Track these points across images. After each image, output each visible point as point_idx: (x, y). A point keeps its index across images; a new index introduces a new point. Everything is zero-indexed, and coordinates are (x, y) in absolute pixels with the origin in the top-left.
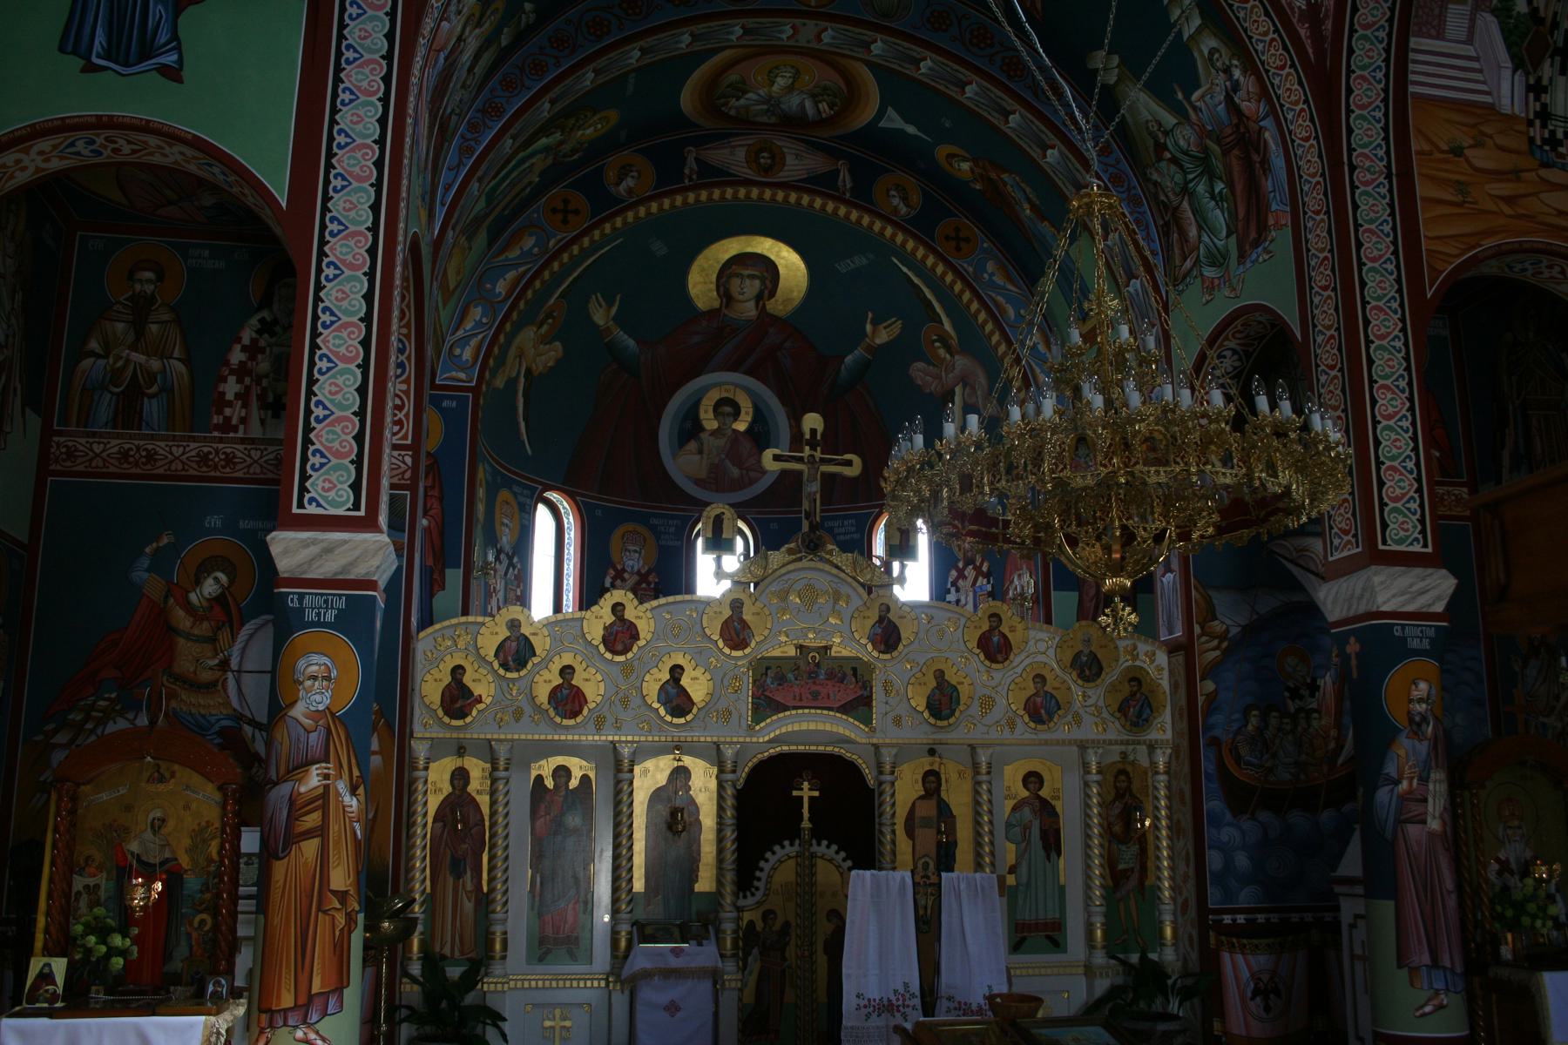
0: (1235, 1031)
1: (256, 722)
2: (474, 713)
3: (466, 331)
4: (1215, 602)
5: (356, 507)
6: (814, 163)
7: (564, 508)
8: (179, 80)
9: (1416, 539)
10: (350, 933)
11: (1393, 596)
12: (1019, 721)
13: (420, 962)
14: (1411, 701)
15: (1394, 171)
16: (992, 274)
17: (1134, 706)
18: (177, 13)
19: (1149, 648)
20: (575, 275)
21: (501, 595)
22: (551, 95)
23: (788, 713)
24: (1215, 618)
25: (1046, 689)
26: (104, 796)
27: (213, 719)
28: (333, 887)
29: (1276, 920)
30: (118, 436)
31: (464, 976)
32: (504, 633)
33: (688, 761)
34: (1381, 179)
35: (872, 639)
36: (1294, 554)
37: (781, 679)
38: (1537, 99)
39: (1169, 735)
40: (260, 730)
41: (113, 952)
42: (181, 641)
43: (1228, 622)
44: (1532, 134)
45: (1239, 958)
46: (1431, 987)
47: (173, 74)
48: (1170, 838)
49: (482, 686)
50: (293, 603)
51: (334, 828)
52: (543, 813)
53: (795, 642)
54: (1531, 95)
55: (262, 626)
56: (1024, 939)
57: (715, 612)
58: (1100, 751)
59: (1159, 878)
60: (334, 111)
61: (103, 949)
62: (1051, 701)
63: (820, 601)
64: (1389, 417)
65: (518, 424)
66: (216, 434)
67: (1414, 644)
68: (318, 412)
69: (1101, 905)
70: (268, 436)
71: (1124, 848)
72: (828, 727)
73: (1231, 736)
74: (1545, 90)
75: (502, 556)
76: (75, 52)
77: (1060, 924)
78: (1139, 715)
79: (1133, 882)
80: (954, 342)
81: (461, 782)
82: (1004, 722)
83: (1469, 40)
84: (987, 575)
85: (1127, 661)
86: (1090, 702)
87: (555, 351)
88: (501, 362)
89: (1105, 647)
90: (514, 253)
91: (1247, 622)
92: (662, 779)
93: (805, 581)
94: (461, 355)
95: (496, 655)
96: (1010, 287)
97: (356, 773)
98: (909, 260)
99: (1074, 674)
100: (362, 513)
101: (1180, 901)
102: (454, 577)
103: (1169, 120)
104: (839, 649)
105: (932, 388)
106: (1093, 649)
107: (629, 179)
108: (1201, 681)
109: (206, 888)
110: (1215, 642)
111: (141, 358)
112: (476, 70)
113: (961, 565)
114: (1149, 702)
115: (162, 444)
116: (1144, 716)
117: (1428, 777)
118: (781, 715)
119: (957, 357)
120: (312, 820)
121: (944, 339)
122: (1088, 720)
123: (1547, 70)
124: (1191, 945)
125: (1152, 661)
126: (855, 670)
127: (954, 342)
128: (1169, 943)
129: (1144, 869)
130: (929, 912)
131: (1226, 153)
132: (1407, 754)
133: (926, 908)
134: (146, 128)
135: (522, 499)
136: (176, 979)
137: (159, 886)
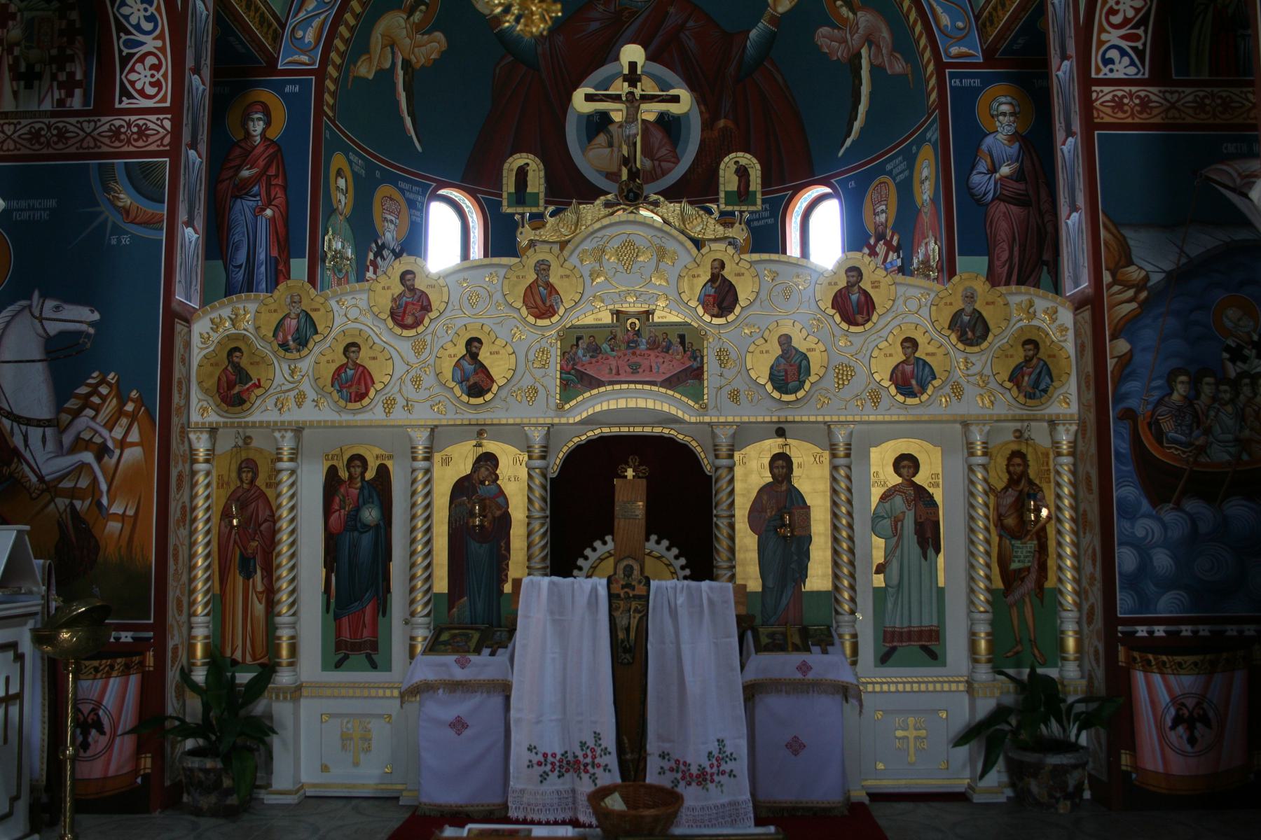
0: (1149, 766)
1: (14, 415)
2: (253, 397)
3: (308, 12)
4: (1131, 243)
7: (468, 207)
12: (884, 394)
13: (206, 668)
17: (1030, 374)
19: (1049, 304)
23: (602, 389)
24: (1130, 263)
25: (917, 355)
29: (1207, 633)
35: (704, 302)
36: (1238, 181)
37: (595, 350)
39: (1074, 409)
40: (19, 423)
43: (1149, 268)
45: (1157, 678)
48: (1075, 532)
52: (337, 508)
53: (612, 307)
55: (19, 312)
56: (893, 649)
57: (518, 277)
58: (987, 428)
59: (1060, 580)
62: (923, 370)
63: (641, 259)
65: (402, 120)
69: (986, 612)
70: (21, 109)
71: (1018, 543)
73: (1150, 407)
75: (385, 253)
77: (938, 632)
78: (1036, 385)
79: (1030, 583)
81: (250, 475)
82: (865, 395)
84: (897, 250)
85: (1021, 320)
86: (974, 370)
89: (993, 303)
91: (1175, 267)
92: (465, 468)
93: (624, 237)
94: (303, 37)
95: (275, 335)
99: (954, 338)
101: (1086, 607)
104: (664, 314)
105: (839, 54)
106: (977, 306)
108: (1110, 341)
110: (1131, 293)
113: (872, 241)
114: (1049, 369)
116: (1042, 386)
118: (595, 392)
119: (859, 14)
122: (970, 391)
124: (1097, 660)
125: (1054, 320)
126: (682, 338)
128: (1072, 657)
129: (1043, 568)
130: (632, 635)
133: (628, 629)
135: (411, 196)
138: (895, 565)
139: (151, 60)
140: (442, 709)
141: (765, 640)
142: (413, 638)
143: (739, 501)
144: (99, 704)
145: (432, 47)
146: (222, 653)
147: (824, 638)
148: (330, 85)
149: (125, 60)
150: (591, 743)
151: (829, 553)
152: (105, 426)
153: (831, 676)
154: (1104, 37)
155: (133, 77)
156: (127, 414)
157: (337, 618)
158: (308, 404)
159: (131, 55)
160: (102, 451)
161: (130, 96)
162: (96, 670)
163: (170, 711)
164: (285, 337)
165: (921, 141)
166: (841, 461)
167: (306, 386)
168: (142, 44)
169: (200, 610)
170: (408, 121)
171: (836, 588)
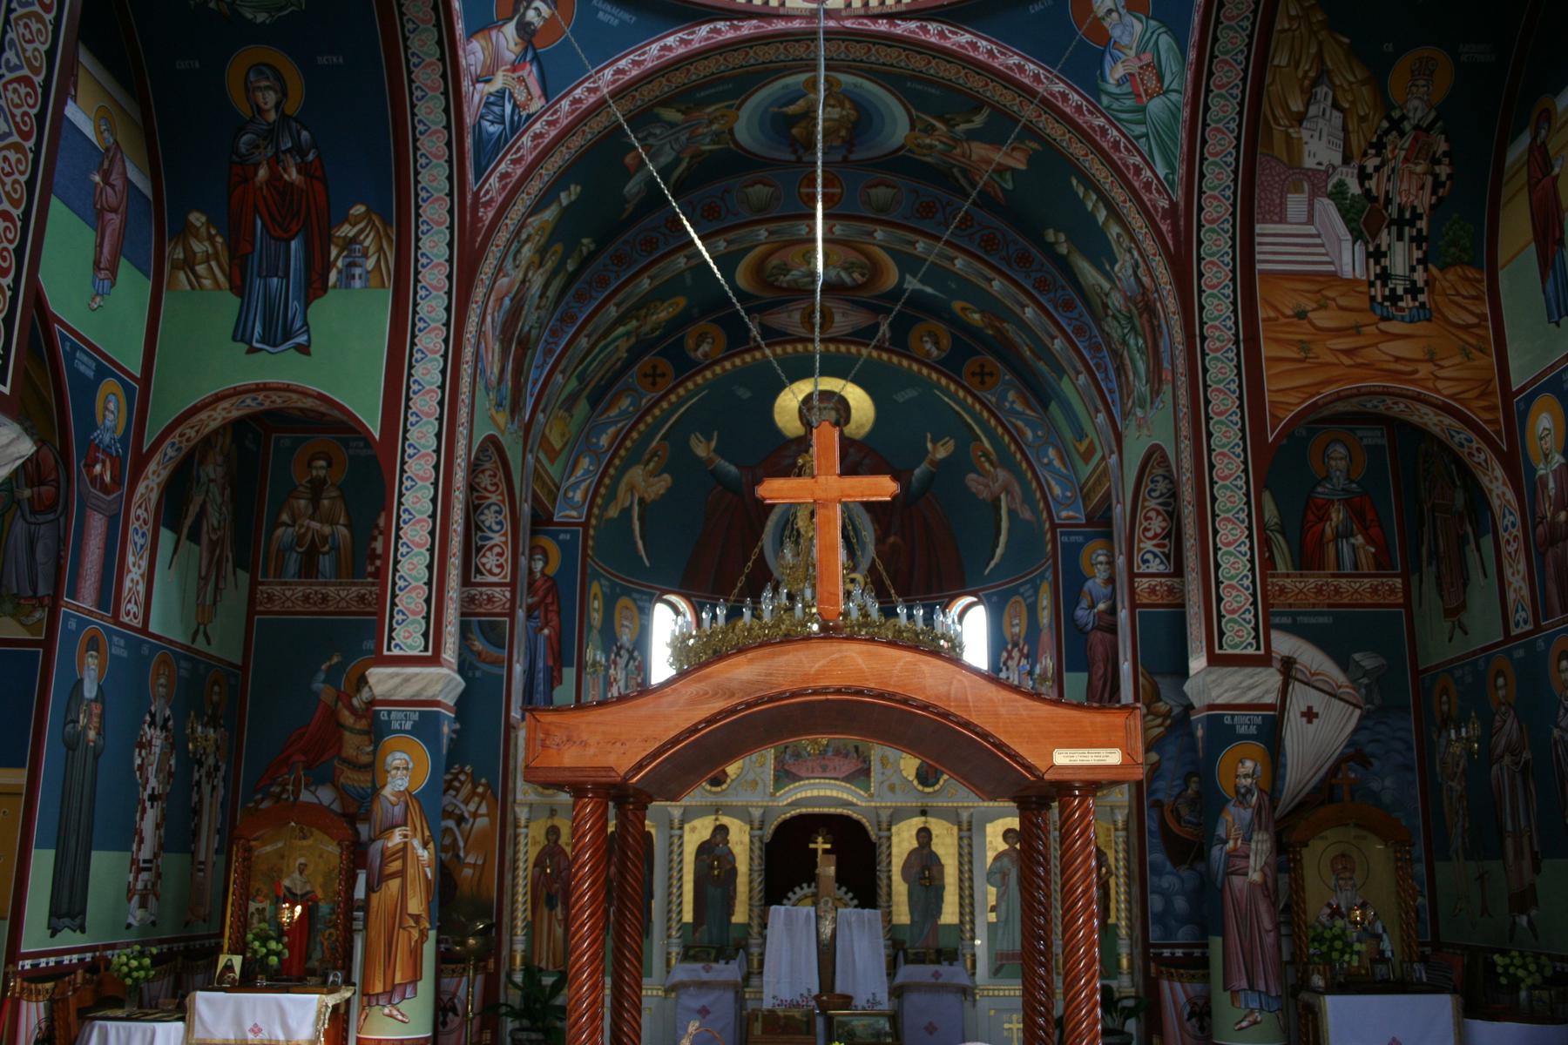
5: (426, 649)
6: (859, 319)
9: (1250, 644)
10: (422, 943)
11: (1226, 691)
14: (1237, 776)
15: (1241, 337)
16: (1013, 402)
20: (671, 422)
21: (622, 684)
22: (616, 300)
24: (1159, 700)
26: (268, 848)
30: (302, 584)
33: (725, 820)
34: (1230, 345)
38: (1377, 263)
41: (270, 952)
42: (347, 734)
43: (1172, 703)
44: (1373, 293)
45: (1177, 986)
46: (1247, 1006)
47: (304, 349)
50: (384, 717)
51: (410, 871)
54: (1372, 261)
56: (1002, 966)
60: (411, 367)
61: (264, 950)
64: (1229, 544)
65: (635, 543)
67: (1242, 730)
68: (401, 583)
72: (835, 794)
74: (1384, 255)
75: (622, 652)
76: (242, 340)
80: (994, 457)
83: (1310, 220)
84: (1027, 657)
88: (612, 495)
90: (613, 413)
92: (706, 834)
96: (1028, 412)
97: (427, 833)
98: (946, 391)
100: (430, 653)
102: (569, 674)
103: (1107, 286)
109: (333, 911)
110: (1159, 721)
111: (315, 525)
113: (1009, 647)
117: (1251, 838)
120: (396, 866)
121: (986, 455)
123: (1384, 238)
127: (994, 457)
131: (1141, 315)
132: (1234, 818)
134: (288, 388)
135: (641, 604)
136: (313, 973)
137: (298, 909)
138: (1003, 907)
139: (497, 550)
140: (692, 1001)
141: (911, 957)
142: (669, 954)
143: (895, 860)
144: (454, 995)
147: (948, 955)
148: (592, 532)
149: (479, 549)
150: (806, 994)
151: (957, 898)
152: (463, 802)
153: (955, 981)
154: (1142, 545)
155: (484, 560)
156: (478, 795)
160: (460, 820)
161: (482, 574)
162: (453, 971)
163: (502, 1000)
165: (1042, 577)
166: (965, 834)
168: (491, 539)
169: (519, 932)
170: (640, 544)
171: (961, 922)
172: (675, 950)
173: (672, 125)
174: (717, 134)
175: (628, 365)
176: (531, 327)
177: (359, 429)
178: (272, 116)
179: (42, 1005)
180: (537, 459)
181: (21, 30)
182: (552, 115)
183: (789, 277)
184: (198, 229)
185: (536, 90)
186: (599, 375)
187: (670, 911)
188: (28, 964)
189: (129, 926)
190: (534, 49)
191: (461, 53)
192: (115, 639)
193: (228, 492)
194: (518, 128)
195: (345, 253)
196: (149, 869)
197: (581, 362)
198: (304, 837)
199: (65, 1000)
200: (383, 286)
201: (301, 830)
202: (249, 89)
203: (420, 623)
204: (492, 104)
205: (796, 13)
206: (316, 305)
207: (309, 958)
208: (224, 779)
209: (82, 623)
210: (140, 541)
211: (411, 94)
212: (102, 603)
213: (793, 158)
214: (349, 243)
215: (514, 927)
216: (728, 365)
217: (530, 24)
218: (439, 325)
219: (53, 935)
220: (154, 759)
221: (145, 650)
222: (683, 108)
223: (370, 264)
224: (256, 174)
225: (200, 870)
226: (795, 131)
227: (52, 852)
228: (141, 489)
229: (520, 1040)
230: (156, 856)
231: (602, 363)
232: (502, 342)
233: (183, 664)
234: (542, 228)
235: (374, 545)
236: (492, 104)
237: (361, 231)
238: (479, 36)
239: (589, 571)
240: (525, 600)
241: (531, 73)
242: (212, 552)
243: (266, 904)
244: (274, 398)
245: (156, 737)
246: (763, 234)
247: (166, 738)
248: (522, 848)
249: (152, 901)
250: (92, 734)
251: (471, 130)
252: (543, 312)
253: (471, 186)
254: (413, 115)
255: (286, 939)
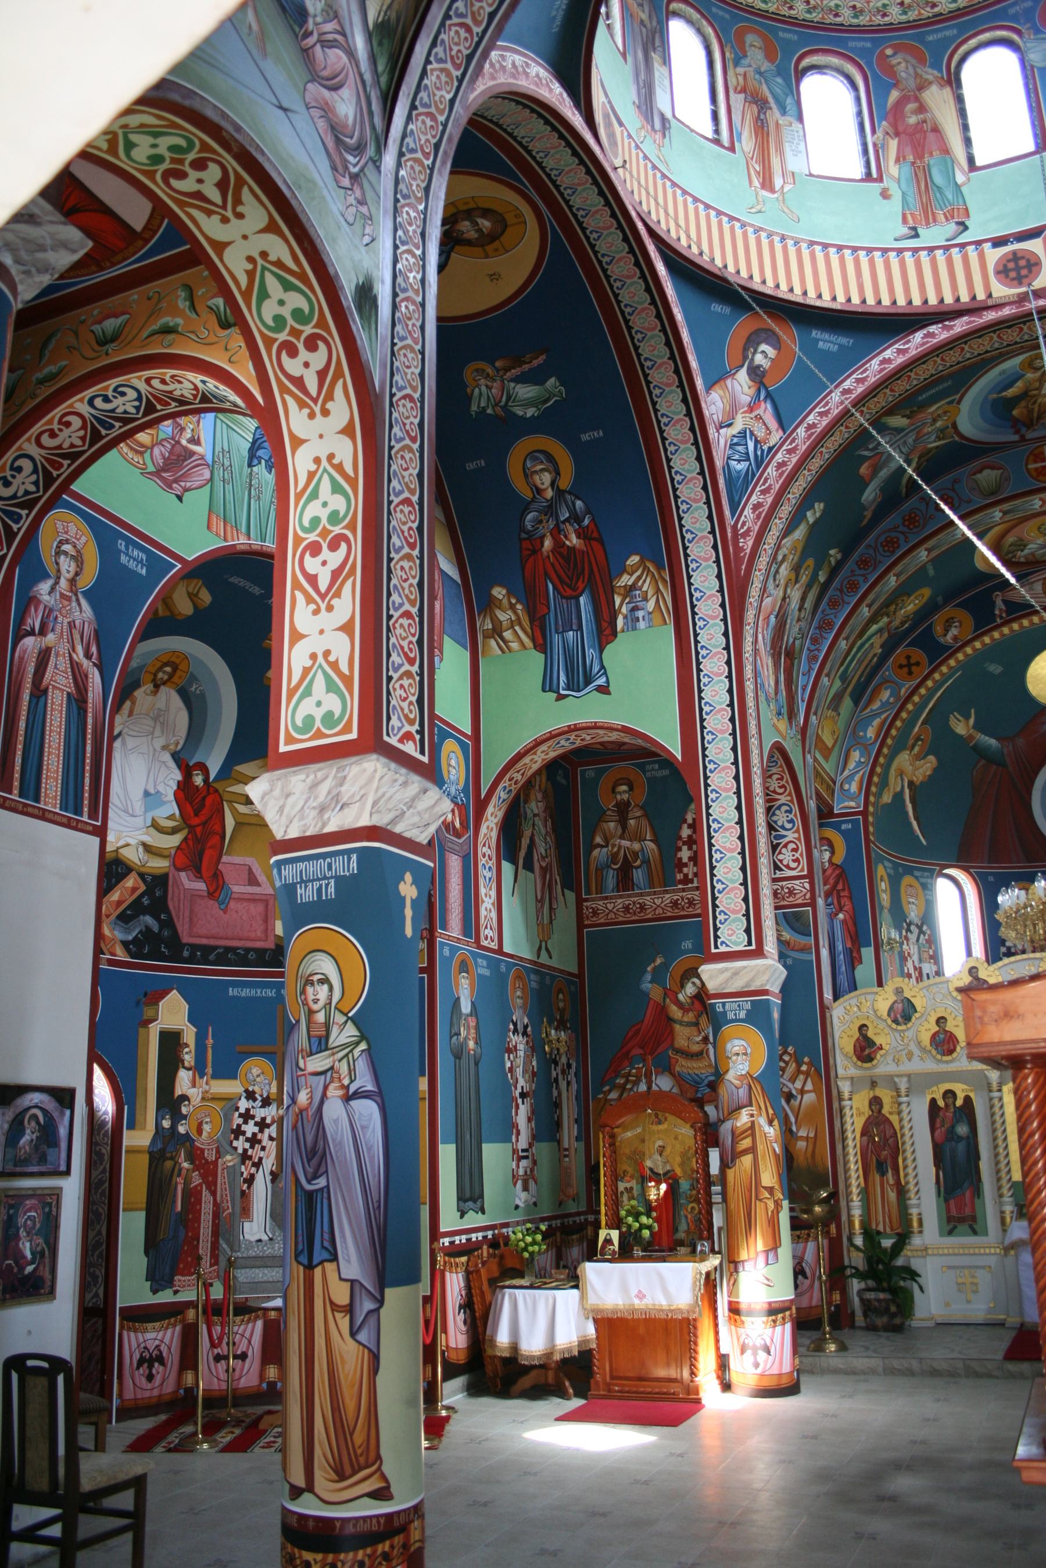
2: (878, 1056)
5: (750, 943)
8: (608, 693)
10: (778, 1213)
18: (601, 651)
21: (915, 958)
26: (629, 1134)
27: (703, 1077)
28: (764, 1184)
30: (621, 897)
31: (894, 1246)
32: (892, 998)
41: (642, 1227)
42: (677, 1027)
47: (604, 690)
49: (883, 1036)
51: (760, 1148)
60: (700, 691)
61: (637, 1225)
65: (910, 824)
66: (680, 886)
75: (912, 927)
76: (551, 690)
87: (930, 763)
88: (884, 784)
90: (876, 705)
95: (889, 1015)
97: (771, 1112)
100: (753, 947)
102: (868, 953)
107: (953, 629)
109: (692, 1187)
111: (626, 843)
112: (806, 606)
115: (648, 898)
120: (746, 1143)
134: (596, 726)
135: (923, 880)
136: (681, 1243)
137: (663, 1187)
139: (792, 846)
145: (928, 766)
146: (870, 1224)
148: (871, 819)
152: (789, 1080)
155: (781, 857)
156: (803, 1073)
157: (946, 1201)
158: (915, 1059)
159: (779, 844)
161: (781, 870)
163: (846, 1263)
164: (895, 1016)
167: (913, 1047)
168: (785, 836)
169: (855, 1198)
172: (1008, 1209)
173: (898, 430)
174: (942, 430)
175: (883, 658)
176: (795, 639)
177: (658, 751)
178: (549, 494)
179: (460, 1275)
180: (815, 760)
181: (400, 461)
182: (791, 444)
183: (1026, 552)
184: (501, 600)
185: (773, 424)
186: (859, 672)
187: (998, 1171)
188: (446, 1241)
189: (517, 1207)
190: (766, 389)
191: (703, 405)
192: (479, 960)
193: (549, 823)
194: (762, 461)
195: (627, 600)
196: (526, 1157)
197: (842, 664)
198: (660, 1123)
199: (478, 1271)
200: (665, 623)
201: (657, 1116)
202: (527, 475)
203: (741, 921)
204: (737, 444)
205: (1003, 301)
206: (609, 649)
207: (676, 1230)
208: (576, 1074)
209: (454, 950)
210: (488, 875)
211: (666, 450)
212: (466, 931)
213: (1016, 438)
214: (630, 589)
215: (849, 1194)
216: (978, 645)
217: (759, 366)
218: (720, 649)
219: (462, 1217)
220: (520, 1061)
221: (503, 968)
222: (908, 413)
223: (651, 605)
224: (542, 545)
225: (566, 1156)
226: (1015, 412)
227: (454, 1146)
228: (483, 830)
229: (869, 1301)
230: (531, 1145)
231: (860, 661)
232: (773, 657)
233: (533, 977)
234: (794, 548)
235: (679, 855)
236: (737, 444)
237: (639, 578)
238: (717, 387)
239: (873, 855)
240: (821, 889)
241: (766, 410)
242: (544, 878)
243: (633, 1184)
244: (584, 736)
245: (518, 1041)
246: (997, 515)
247: (527, 1042)
248: (848, 1119)
249: (531, 1183)
250: (471, 1044)
251: (721, 471)
252: (803, 624)
253: (730, 521)
254: (670, 468)
255: (654, 1214)
